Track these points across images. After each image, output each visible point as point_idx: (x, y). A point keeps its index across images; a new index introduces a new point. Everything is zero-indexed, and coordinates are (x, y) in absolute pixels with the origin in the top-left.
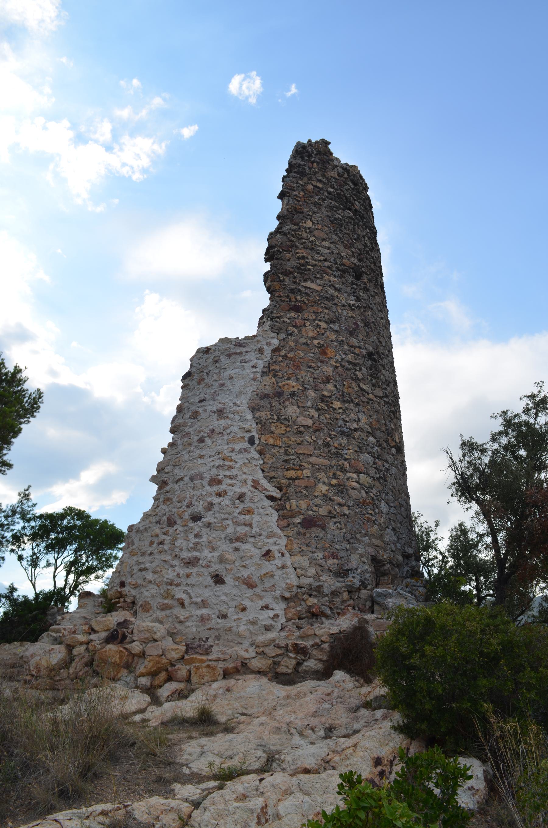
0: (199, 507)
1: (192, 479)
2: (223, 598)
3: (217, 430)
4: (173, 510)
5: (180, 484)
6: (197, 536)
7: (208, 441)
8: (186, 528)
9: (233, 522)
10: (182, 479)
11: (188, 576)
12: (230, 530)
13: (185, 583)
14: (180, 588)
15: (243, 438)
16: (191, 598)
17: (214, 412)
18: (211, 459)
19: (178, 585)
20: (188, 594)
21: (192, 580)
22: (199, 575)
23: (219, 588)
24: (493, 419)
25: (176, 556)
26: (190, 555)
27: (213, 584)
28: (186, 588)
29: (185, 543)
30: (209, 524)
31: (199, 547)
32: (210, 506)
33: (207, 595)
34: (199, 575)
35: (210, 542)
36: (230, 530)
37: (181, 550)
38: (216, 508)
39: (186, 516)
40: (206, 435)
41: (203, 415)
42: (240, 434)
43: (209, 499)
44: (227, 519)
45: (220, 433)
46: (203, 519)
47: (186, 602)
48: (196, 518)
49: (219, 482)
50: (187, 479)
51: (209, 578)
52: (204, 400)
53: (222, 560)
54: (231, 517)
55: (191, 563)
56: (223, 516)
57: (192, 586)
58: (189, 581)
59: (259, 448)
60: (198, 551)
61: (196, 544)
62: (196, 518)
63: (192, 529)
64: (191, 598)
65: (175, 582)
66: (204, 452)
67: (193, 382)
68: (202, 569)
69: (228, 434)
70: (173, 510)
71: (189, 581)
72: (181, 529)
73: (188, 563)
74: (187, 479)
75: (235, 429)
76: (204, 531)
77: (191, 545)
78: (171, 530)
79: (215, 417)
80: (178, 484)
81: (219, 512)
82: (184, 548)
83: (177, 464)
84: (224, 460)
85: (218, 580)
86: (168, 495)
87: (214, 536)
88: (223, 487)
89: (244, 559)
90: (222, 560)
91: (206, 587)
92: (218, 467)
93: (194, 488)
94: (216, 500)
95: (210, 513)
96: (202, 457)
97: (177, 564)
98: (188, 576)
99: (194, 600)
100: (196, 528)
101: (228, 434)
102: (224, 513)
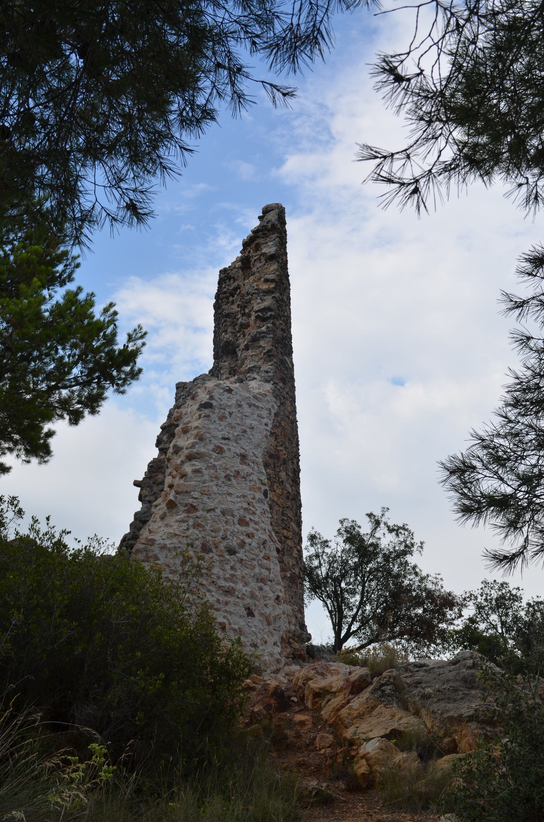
0: (234, 543)
1: (223, 513)
2: (254, 629)
3: (242, 474)
4: (207, 537)
5: (212, 513)
6: (232, 568)
7: (234, 481)
8: (222, 558)
9: (259, 564)
10: (213, 510)
11: (227, 603)
12: (257, 570)
13: (224, 609)
14: (220, 613)
15: (260, 488)
16: (230, 624)
17: (237, 455)
18: (239, 500)
19: (217, 610)
20: (228, 619)
21: (229, 608)
22: (235, 604)
23: (250, 619)
24: (67, 530)
25: (213, 582)
26: (228, 584)
27: (246, 615)
28: (225, 614)
29: (221, 573)
30: (242, 560)
31: (234, 579)
32: (242, 544)
33: (242, 624)
34: (235, 604)
35: (243, 577)
36: (257, 570)
37: (219, 578)
38: (247, 547)
39: (222, 546)
40: (232, 474)
41: (227, 454)
42: (258, 484)
43: (242, 538)
44: (254, 560)
45: (244, 477)
46: (237, 554)
47: (227, 626)
48: (232, 552)
49: (247, 524)
50: (218, 511)
51: (243, 609)
52: (228, 439)
53: (253, 596)
54: (257, 559)
55: (228, 592)
56: (252, 556)
57: (231, 613)
58: (227, 608)
59: (270, 502)
60: (234, 582)
61: (233, 576)
62: (232, 552)
63: (228, 560)
64: (230, 624)
65: (216, 607)
66: (231, 491)
67: (214, 415)
68: (238, 600)
69: (250, 481)
70: (207, 537)
71: (227, 608)
72: (216, 557)
73: (227, 592)
74: (218, 511)
75: (254, 477)
76: (238, 566)
77: (228, 576)
78: (207, 557)
79: (238, 460)
80: (210, 514)
81: (249, 552)
82: (222, 576)
83: (206, 492)
84: (249, 504)
85: (250, 614)
86: (199, 521)
87: (246, 572)
88: (250, 530)
89: (266, 599)
90: (253, 596)
91: (241, 616)
92: (245, 509)
93: (226, 522)
94: (248, 540)
95: (242, 550)
96: (230, 494)
97: (214, 590)
98: (227, 603)
99: (233, 626)
100: (231, 560)
101: (250, 481)
102: (253, 554)
